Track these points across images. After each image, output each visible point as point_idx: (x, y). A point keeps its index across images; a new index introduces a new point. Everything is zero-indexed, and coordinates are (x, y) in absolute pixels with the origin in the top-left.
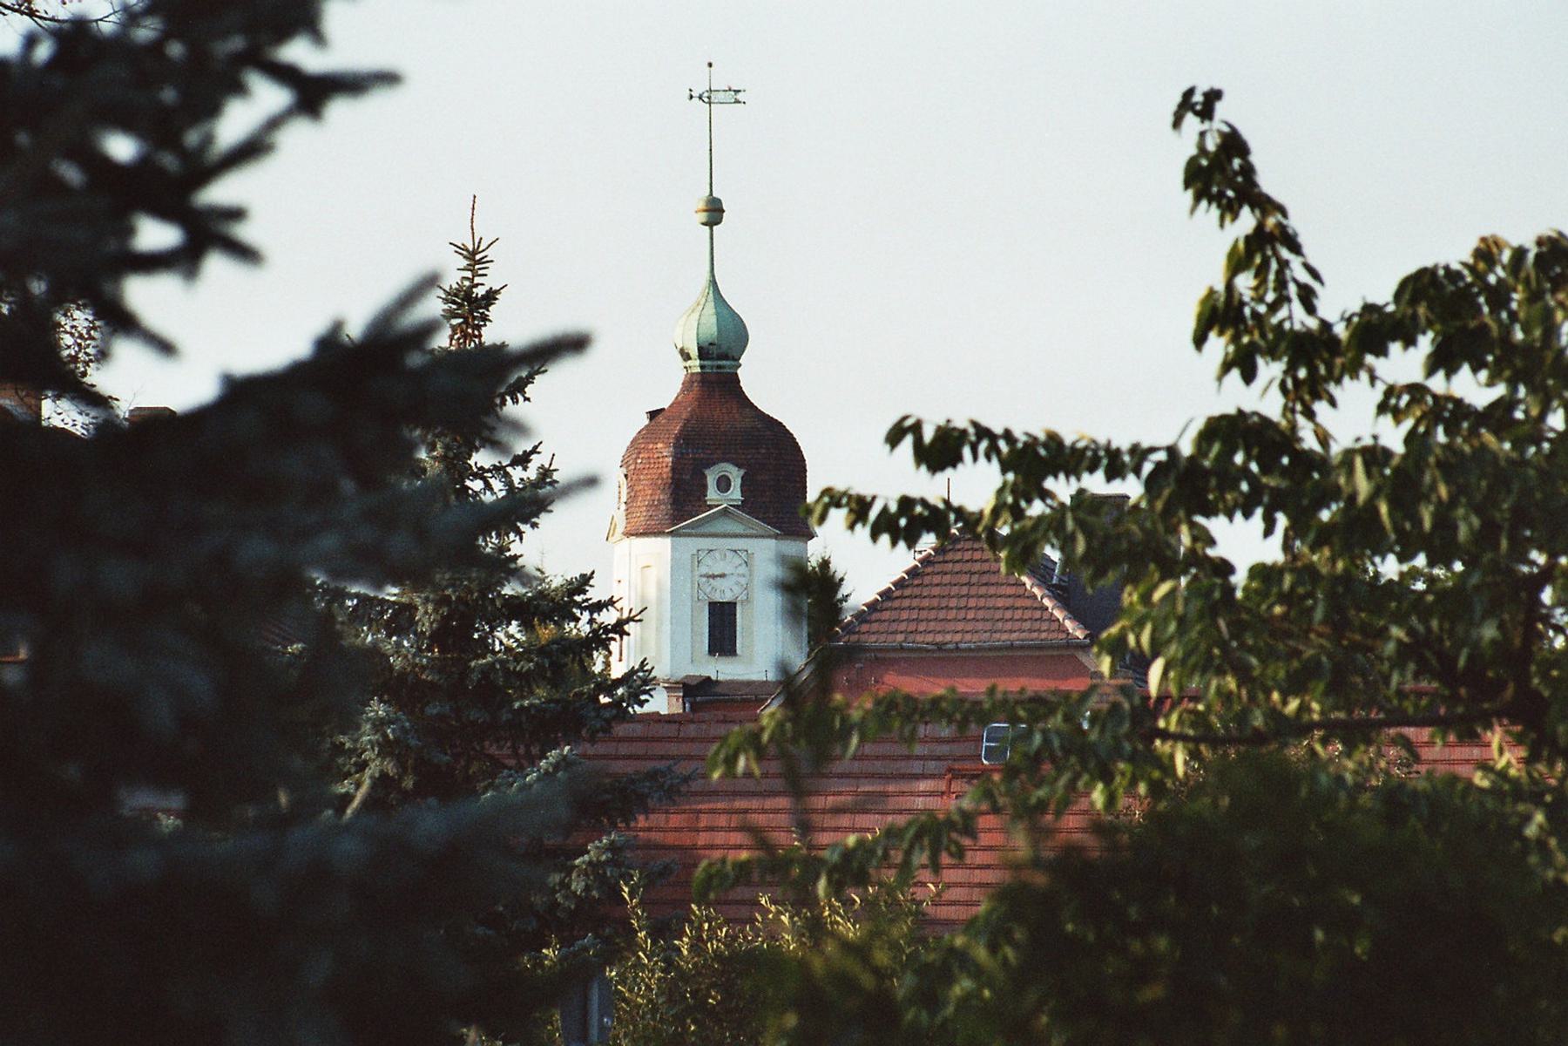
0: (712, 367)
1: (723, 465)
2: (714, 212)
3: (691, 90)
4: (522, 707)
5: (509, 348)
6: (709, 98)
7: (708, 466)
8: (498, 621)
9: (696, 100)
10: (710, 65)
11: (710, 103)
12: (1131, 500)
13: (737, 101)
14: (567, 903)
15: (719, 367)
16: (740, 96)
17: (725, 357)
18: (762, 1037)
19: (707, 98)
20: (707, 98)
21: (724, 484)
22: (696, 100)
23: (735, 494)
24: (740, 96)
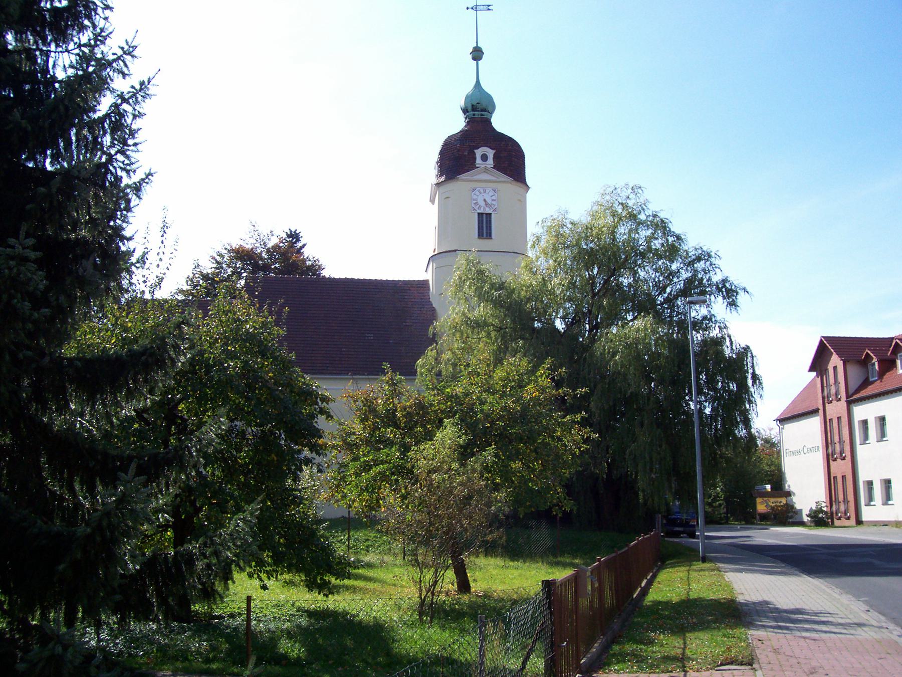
0: (478, 115)
2: (477, 54)
4: (47, 412)
8: (820, 515)
9: (470, 10)
13: (489, 10)
14: (560, 391)
15: (482, 115)
16: (490, 8)
18: (352, 383)
19: (475, 8)
20: (475, 8)
21: (484, 158)
22: (470, 10)
23: (490, 162)
24: (490, 8)
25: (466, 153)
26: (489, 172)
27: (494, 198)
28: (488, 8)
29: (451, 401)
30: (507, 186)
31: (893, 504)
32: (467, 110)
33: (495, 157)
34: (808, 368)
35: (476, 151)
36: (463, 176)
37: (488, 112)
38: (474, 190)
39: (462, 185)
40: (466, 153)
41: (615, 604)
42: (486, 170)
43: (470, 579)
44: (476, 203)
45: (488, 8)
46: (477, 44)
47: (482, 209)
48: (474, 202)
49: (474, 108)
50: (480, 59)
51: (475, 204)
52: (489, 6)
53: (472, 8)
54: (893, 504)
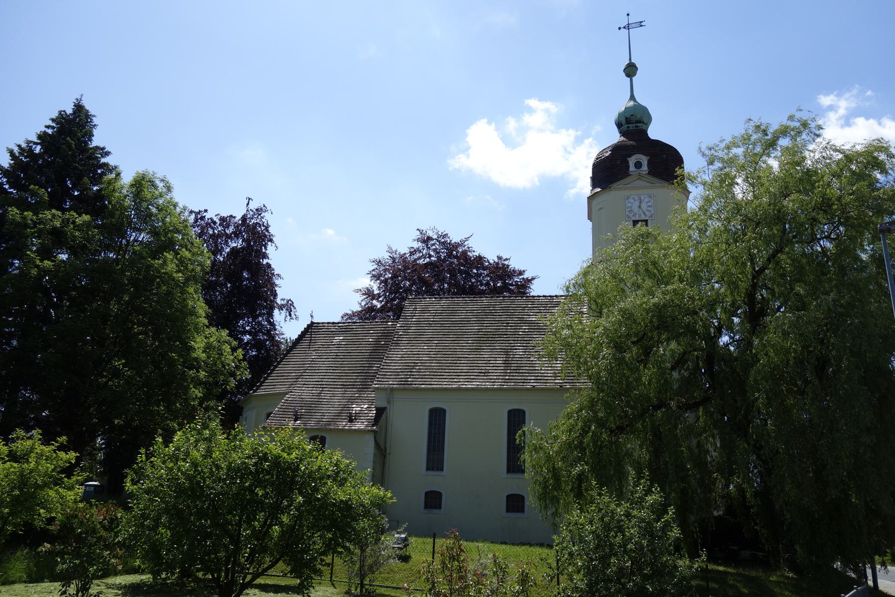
1: (257, 590)
2: (631, 70)
3: (620, 28)
5: (485, 120)
6: (628, 27)
7: (630, 156)
10: (628, 15)
11: (629, 29)
12: (462, 158)
13: (641, 26)
15: (636, 127)
16: (642, 24)
17: (640, 122)
20: (628, 27)
21: (638, 165)
23: (645, 167)
24: (642, 24)
25: (619, 163)
26: (643, 178)
27: (650, 204)
28: (640, 24)
29: (258, 326)
30: (664, 192)
31: (437, 418)
32: (621, 124)
33: (650, 163)
34: (88, 105)
35: (629, 159)
36: (615, 185)
37: (643, 123)
38: (628, 198)
39: (616, 194)
40: (619, 163)
41: (869, 572)
42: (640, 177)
43: (425, 540)
44: (631, 211)
45: (640, 24)
46: (630, 59)
47: (637, 216)
48: (629, 210)
49: (628, 121)
50: (635, 74)
51: (629, 211)
52: (641, 22)
53: (624, 28)
54: (437, 418)
